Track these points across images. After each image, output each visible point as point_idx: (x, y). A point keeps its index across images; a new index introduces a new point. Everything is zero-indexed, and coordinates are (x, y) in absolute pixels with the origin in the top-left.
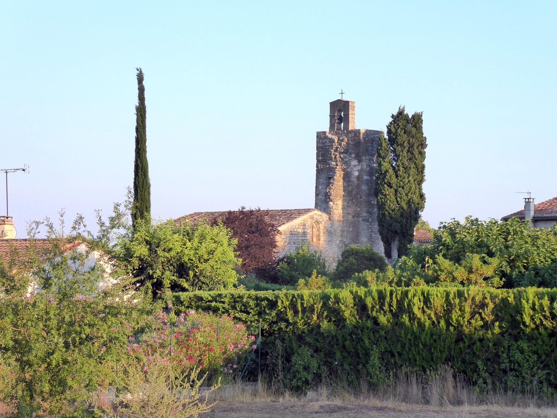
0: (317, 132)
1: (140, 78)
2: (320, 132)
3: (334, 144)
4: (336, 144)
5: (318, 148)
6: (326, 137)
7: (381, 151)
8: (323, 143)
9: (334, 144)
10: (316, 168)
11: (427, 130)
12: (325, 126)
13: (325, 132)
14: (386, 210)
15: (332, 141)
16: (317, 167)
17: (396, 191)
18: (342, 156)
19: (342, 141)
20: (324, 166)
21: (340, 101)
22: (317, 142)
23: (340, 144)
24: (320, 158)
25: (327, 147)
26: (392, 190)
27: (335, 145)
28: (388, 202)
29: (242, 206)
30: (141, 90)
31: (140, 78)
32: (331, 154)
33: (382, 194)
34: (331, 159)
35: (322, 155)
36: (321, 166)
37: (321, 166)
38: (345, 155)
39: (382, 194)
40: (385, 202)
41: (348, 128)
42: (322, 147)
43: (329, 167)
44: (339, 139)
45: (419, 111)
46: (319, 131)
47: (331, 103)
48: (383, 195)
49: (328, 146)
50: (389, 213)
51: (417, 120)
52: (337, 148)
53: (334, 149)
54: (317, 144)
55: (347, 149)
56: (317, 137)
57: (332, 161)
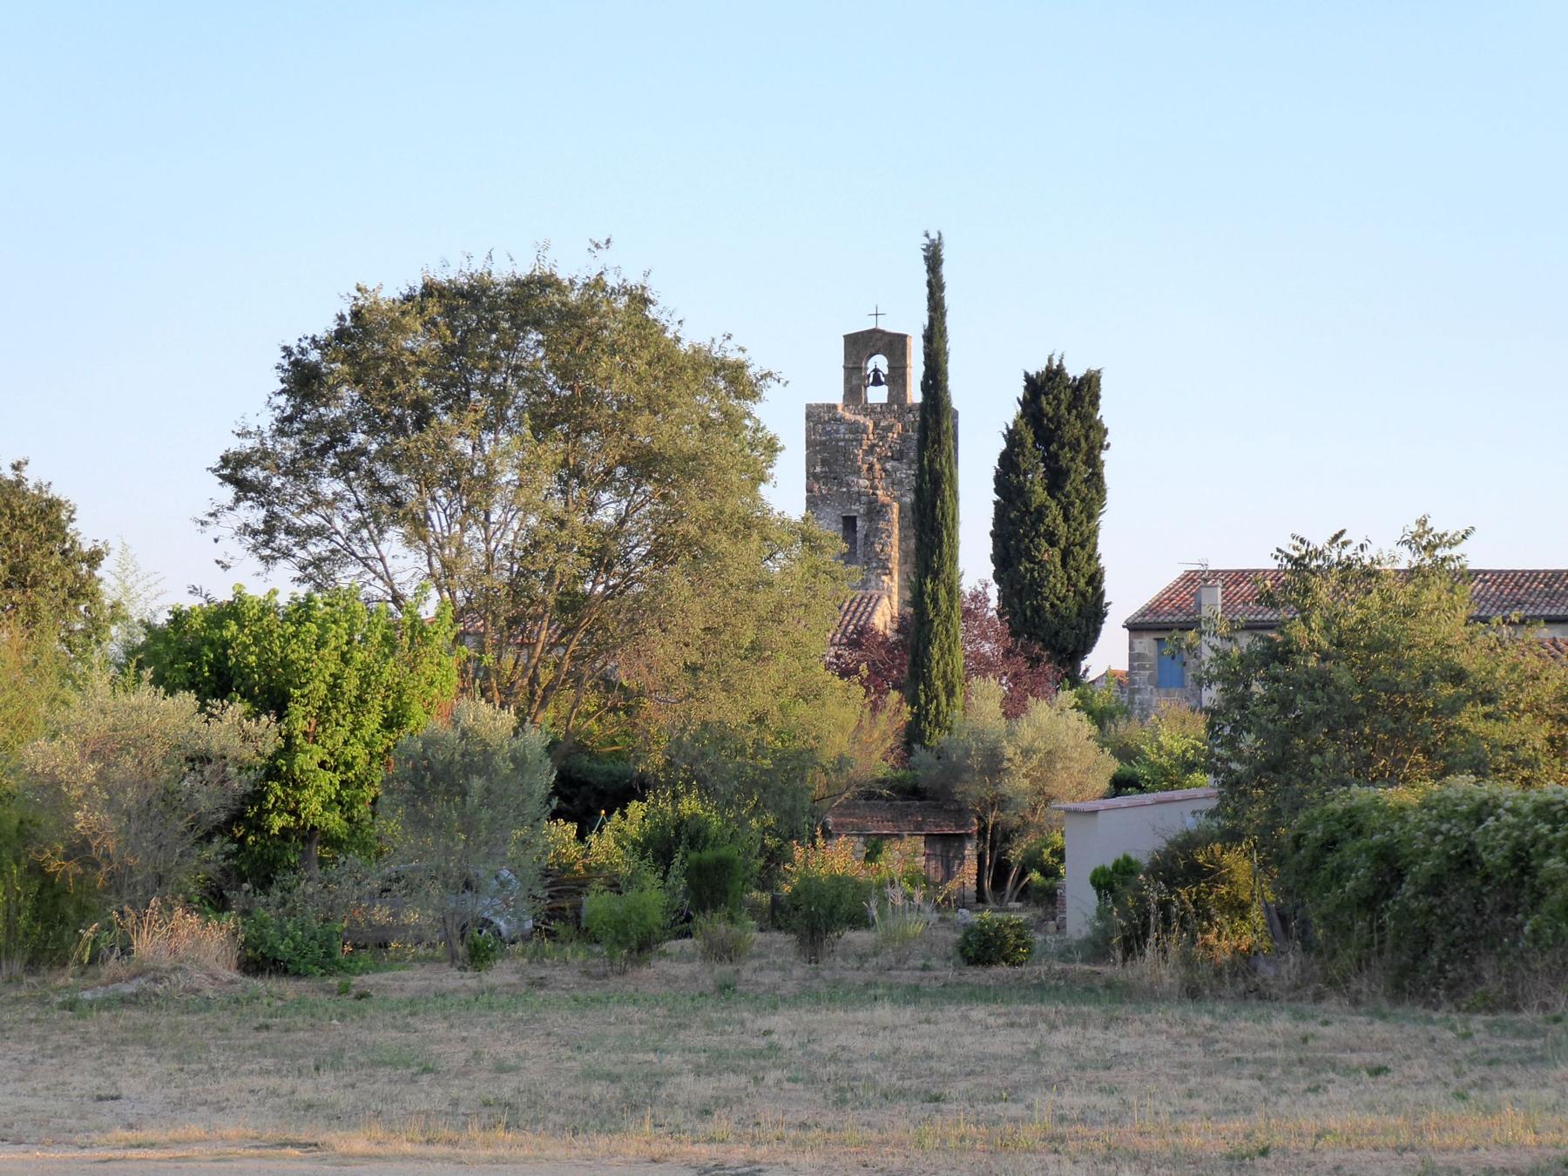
0: (809, 406)
1: (934, 260)
2: (818, 406)
3: (865, 436)
4: (871, 436)
5: (809, 444)
6: (840, 420)
7: (1021, 459)
8: (829, 433)
9: (865, 436)
10: (804, 494)
11: (1108, 411)
12: (832, 391)
13: (835, 407)
14: (1046, 599)
15: (856, 429)
16: (809, 490)
17: (1065, 555)
18: (888, 466)
19: (890, 428)
20: (830, 489)
21: (878, 335)
22: (808, 430)
23: (882, 438)
24: (818, 469)
25: (841, 444)
26: (1056, 553)
27: (870, 438)
28: (1051, 578)
29: (277, 588)
30: (935, 288)
31: (934, 260)
32: (854, 461)
33: (1032, 560)
34: (857, 472)
35: (824, 462)
36: (821, 488)
37: (821, 488)
38: (895, 463)
39: (1032, 560)
40: (1042, 579)
41: (905, 399)
42: (823, 443)
43: (849, 491)
44: (876, 425)
45: (1095, 368)
46: (813, 402)
47: (847, 338)
48: (1035, 563)
49: (843, 440)
50: (1052, 605)
51: (1087, 390)
52: (873, 446)
53: (865, 447)
54: (808, 436)
55: (901, 452)
56: (808, 417)
57: (860, 477)
